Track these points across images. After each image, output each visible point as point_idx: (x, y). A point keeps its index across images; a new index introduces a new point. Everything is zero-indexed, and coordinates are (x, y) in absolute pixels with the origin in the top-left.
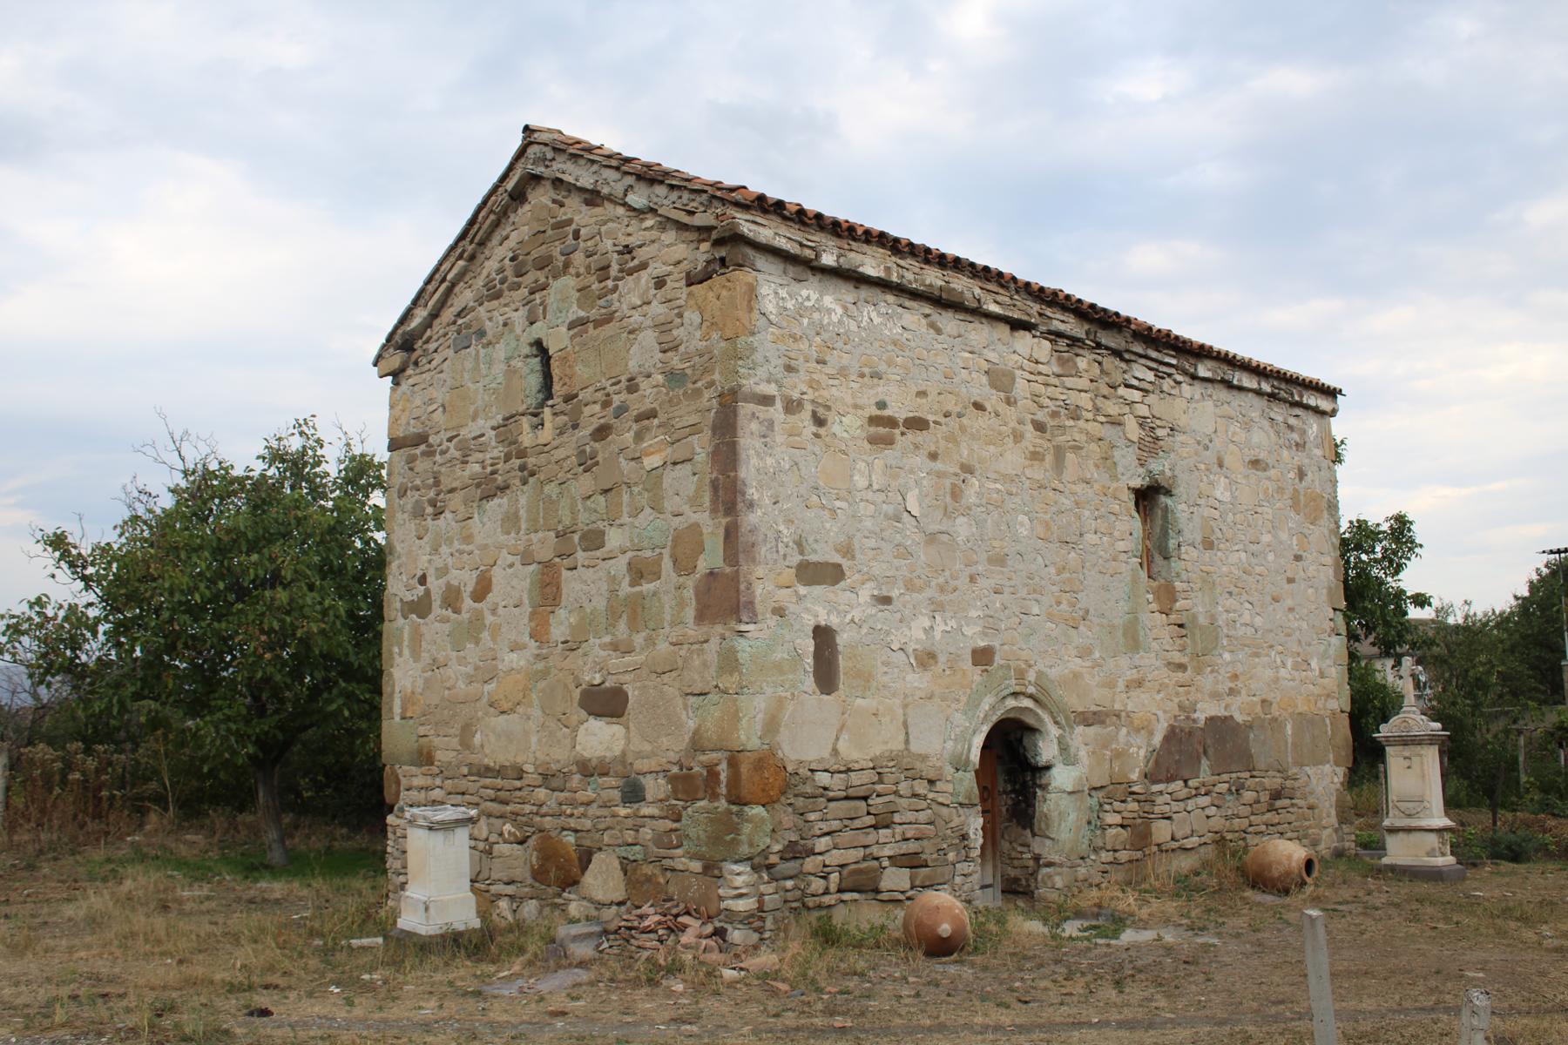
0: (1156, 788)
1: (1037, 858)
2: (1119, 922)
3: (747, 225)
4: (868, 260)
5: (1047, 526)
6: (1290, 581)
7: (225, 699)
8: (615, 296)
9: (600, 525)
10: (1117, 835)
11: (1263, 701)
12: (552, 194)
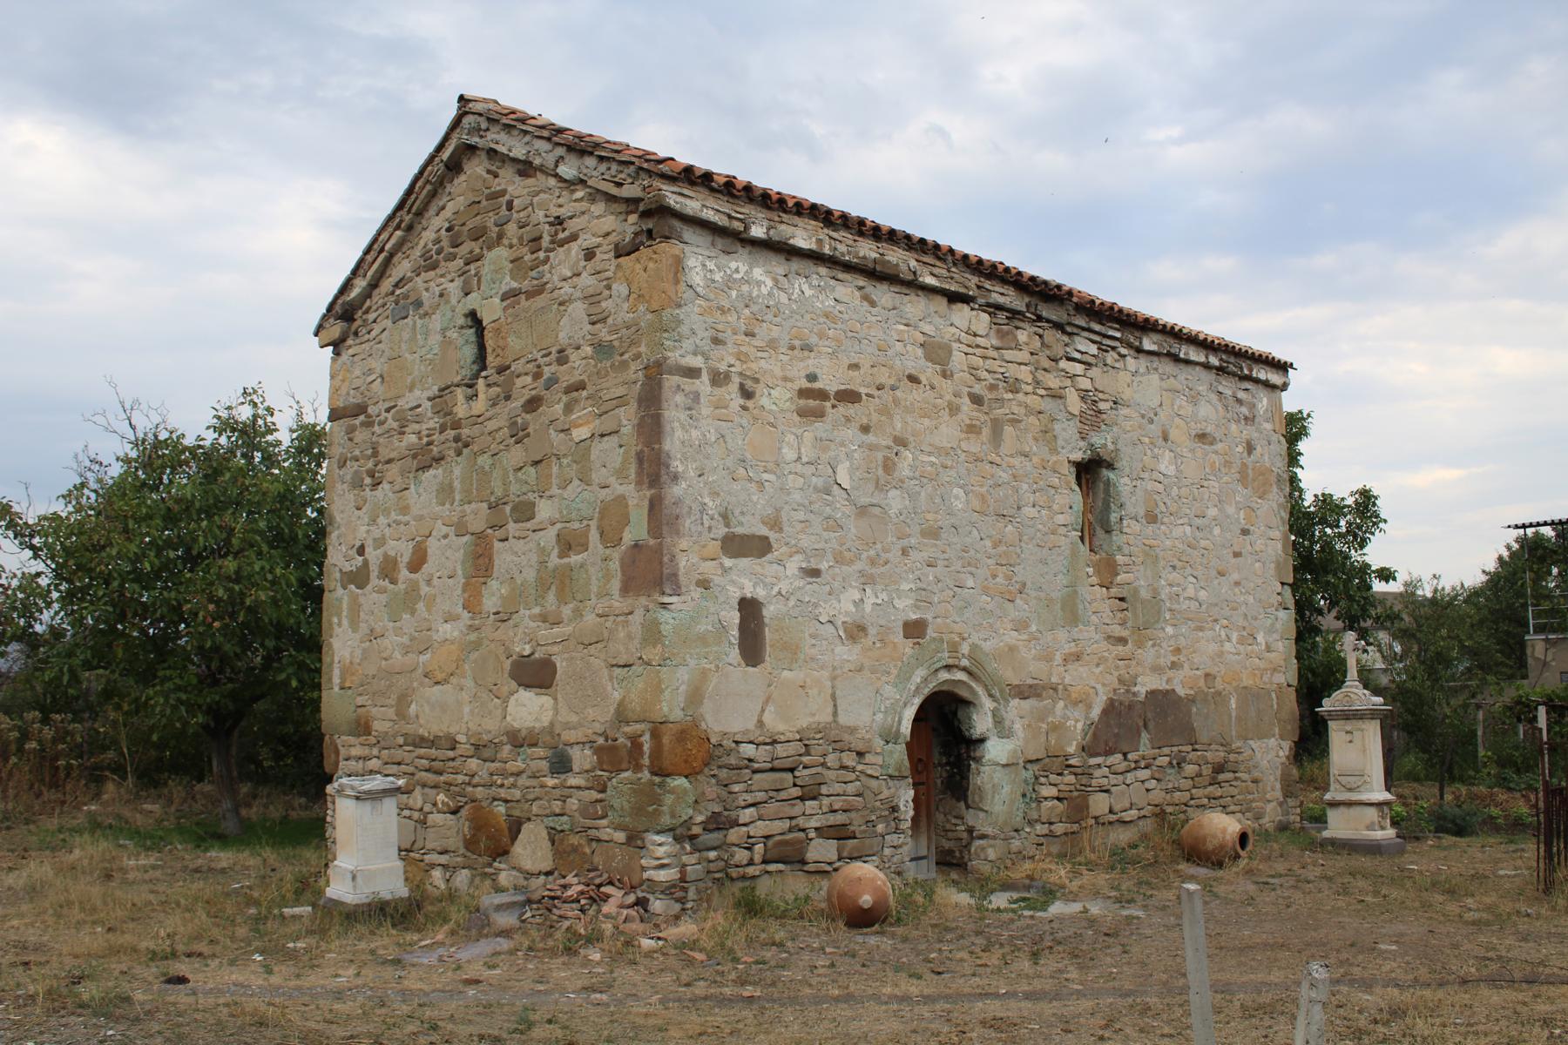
0: (1093, 761)
1: (970, 830)
2: (1050, 894)
3: (673, 197)
4: (799, 232)
5: (983, 499)
6: (1237, 555)
7: (175, 669)
8: (547, 267)
9: (531, 496)
10: (1052, 808)
11: (1207, 675)
12: (486, 164)
